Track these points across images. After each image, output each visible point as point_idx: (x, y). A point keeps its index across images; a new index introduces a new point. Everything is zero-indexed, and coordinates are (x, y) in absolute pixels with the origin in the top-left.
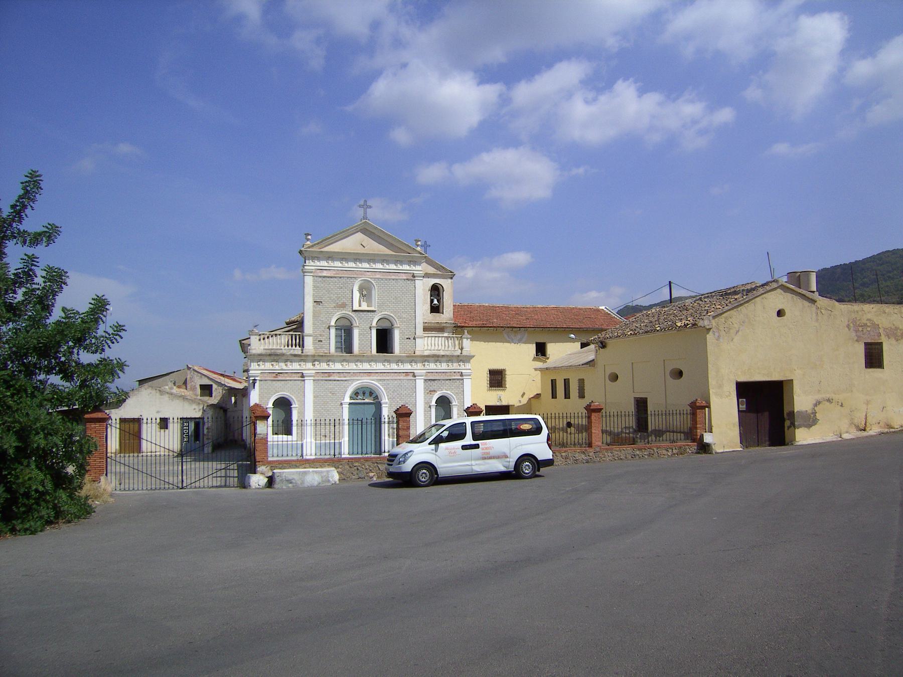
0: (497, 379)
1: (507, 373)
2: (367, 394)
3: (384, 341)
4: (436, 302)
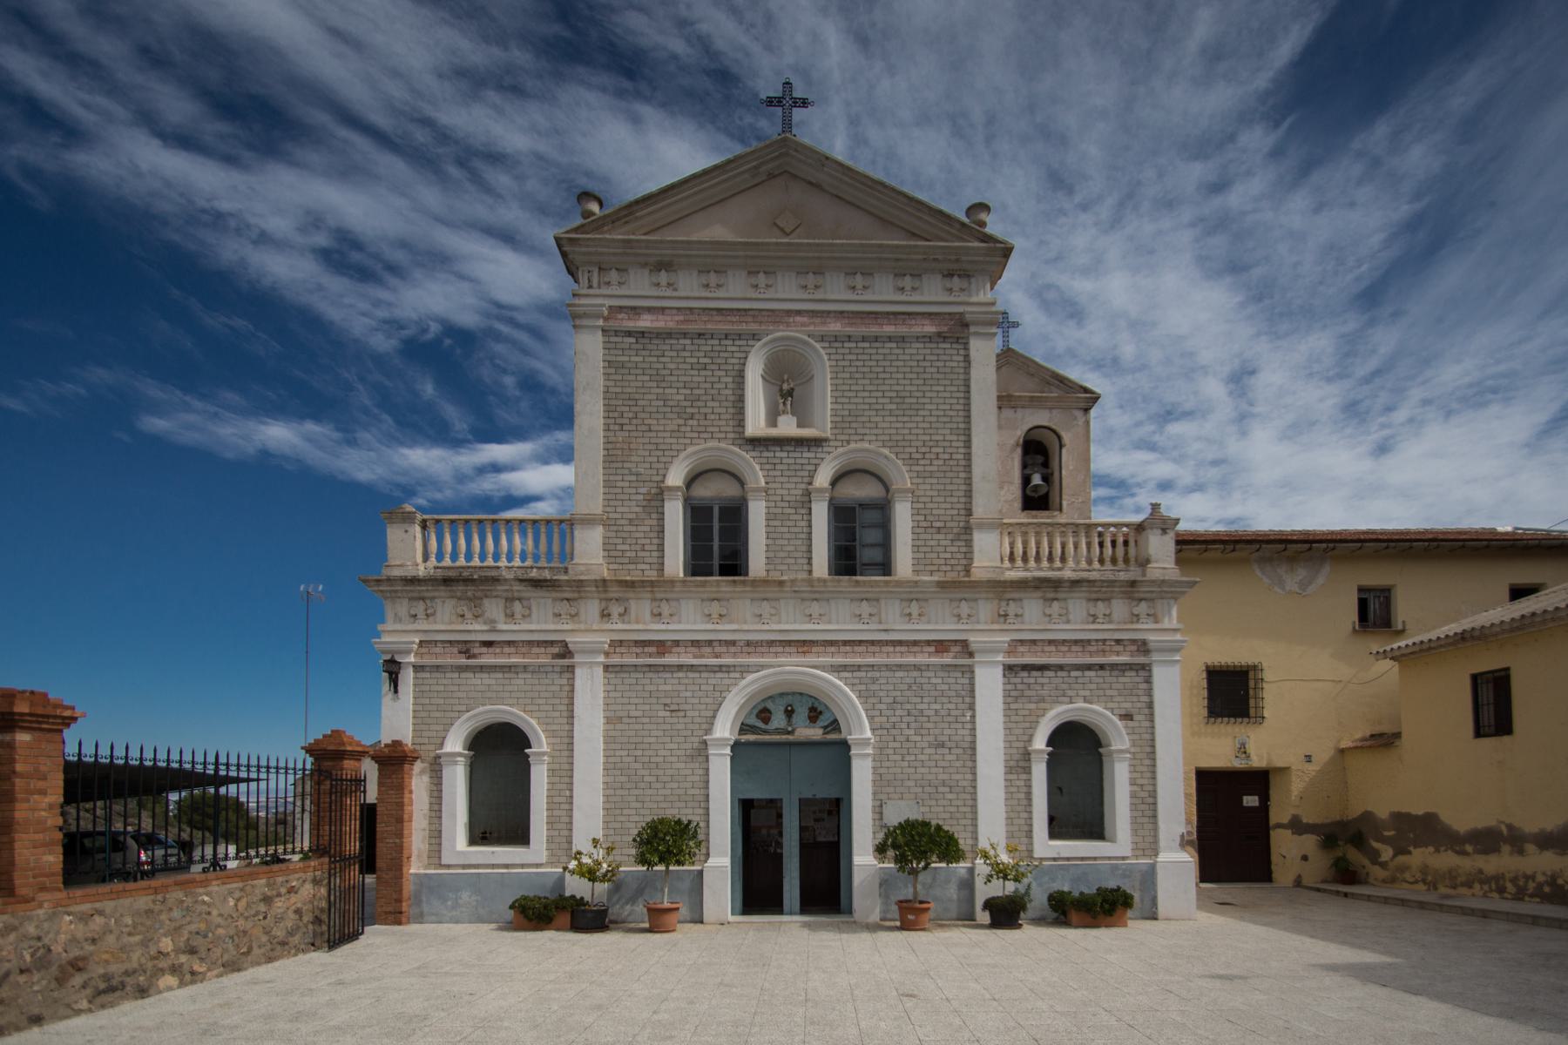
0: (1230, 693)
1: (1267, 675)
2: (802, 714)
3: (858, 546)
4: (1037, 480)
